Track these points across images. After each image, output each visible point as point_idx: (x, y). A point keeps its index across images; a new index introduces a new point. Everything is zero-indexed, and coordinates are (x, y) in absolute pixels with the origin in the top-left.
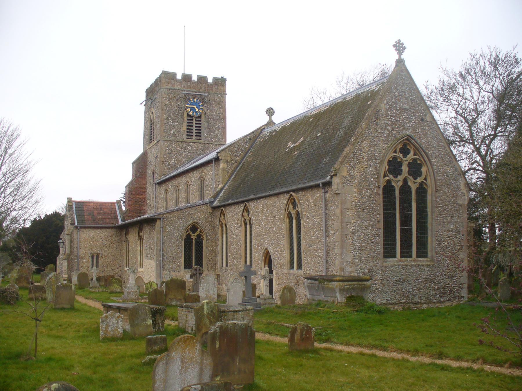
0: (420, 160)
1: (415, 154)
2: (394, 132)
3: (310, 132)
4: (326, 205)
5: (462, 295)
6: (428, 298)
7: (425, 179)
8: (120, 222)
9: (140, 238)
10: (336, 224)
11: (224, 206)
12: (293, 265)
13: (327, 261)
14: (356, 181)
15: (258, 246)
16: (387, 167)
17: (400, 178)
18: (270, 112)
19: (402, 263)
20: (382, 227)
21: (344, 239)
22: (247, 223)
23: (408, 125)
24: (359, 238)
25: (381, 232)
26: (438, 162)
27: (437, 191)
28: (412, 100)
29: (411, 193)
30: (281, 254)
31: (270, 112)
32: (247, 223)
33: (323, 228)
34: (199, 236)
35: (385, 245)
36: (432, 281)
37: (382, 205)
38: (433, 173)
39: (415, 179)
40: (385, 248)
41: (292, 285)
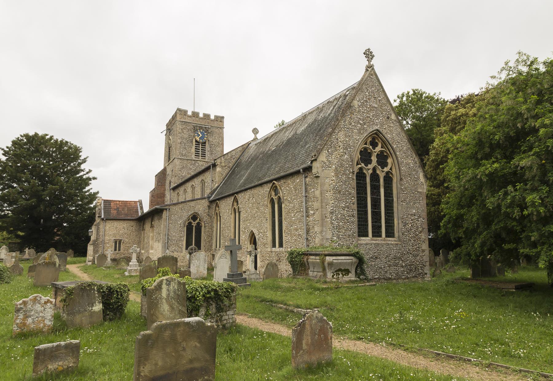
0: (386, 152)
1: (382, 148)
2: (365, 126)
4: (306, 189)
6: (397, 274)
7: (391, 169)
9: (152, 226)
10: (316, 205)
11: (219, 199)
12: (275, 244)
13: (307, 239)
14: (334, 166)
15: (245, 229)
16: (359, 157)
17: (370, 166)
18: (255, 131)
19: (374, 242)
21: (323, 218)
22: (236, 211)
25: (355, 213)
27: (401, 179)
28: (379, 101)
30: (265, 235)
31: (255, 131)
32: (236, 211)
34: (198, 224)
35: (359, 225)
36: (400, 258)
40: (359, 228)
41: (274, 261)
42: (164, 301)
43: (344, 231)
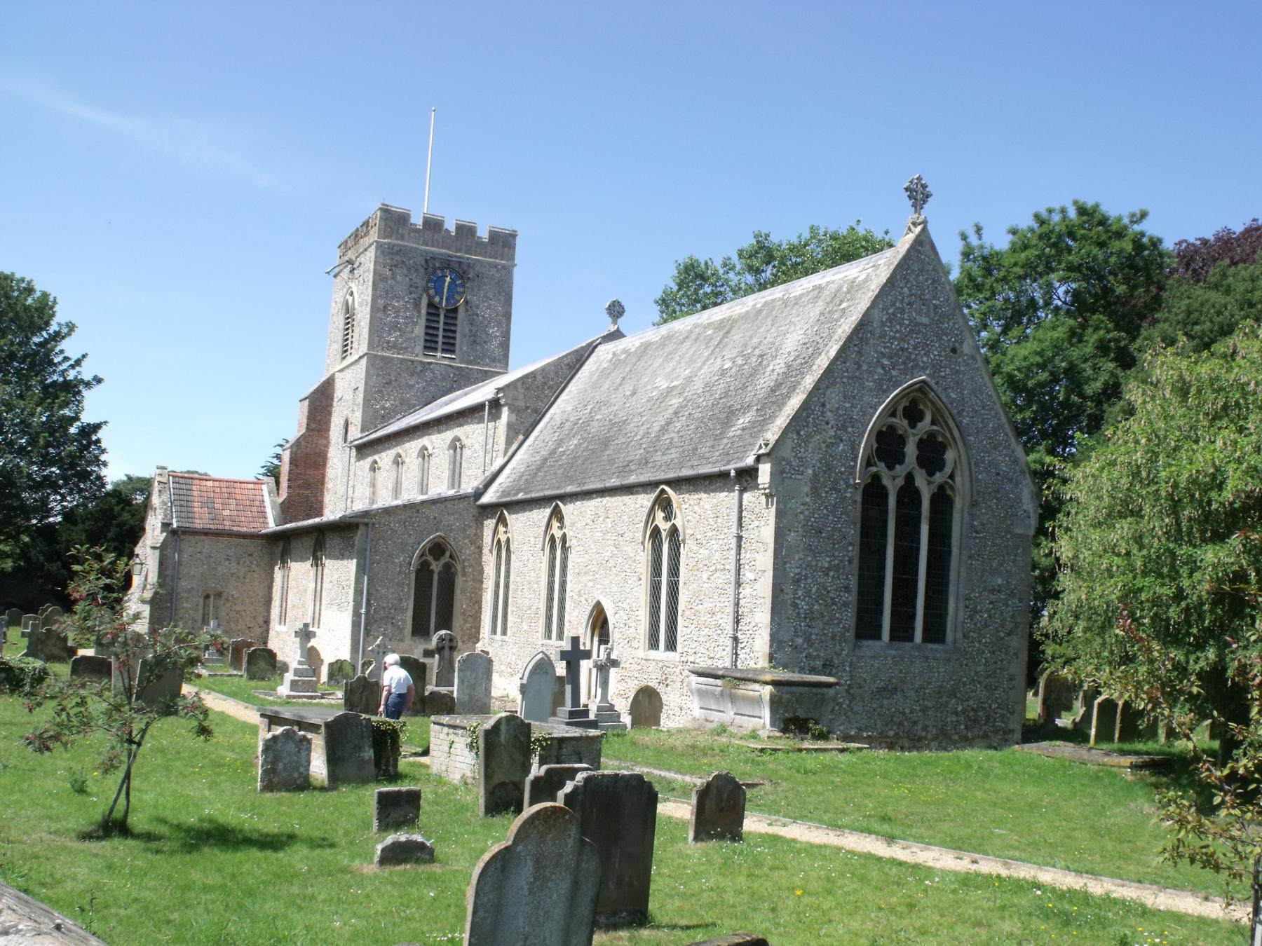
1: (933, 423)
2: (894, 373)
3: (707, 360)
5: (1011, 727)
8: (272, 526)
14: (810, 471)
20: (856, 572)
22: (557, 547)
23: (925, 359)
24: (808, 593)
25: (853, 582)
26: (981, 442)
27: (974, 504)
28: (936, 307)
29: (920, 503)
30: (630, 621)
32: (557, 547)
33: (732, 566)
36: (953, 694)
37: (859, 525)
38: (970, 464)
39: (931, 474)
41: (653, 684)
42: (1081, 694)
43: (821, 625)
